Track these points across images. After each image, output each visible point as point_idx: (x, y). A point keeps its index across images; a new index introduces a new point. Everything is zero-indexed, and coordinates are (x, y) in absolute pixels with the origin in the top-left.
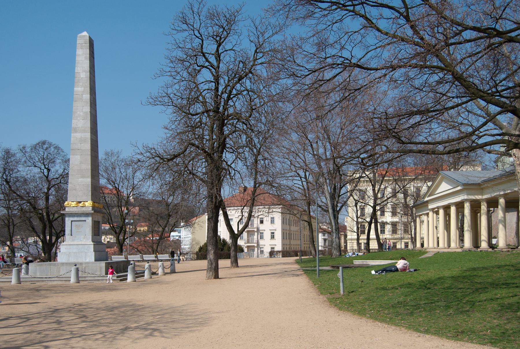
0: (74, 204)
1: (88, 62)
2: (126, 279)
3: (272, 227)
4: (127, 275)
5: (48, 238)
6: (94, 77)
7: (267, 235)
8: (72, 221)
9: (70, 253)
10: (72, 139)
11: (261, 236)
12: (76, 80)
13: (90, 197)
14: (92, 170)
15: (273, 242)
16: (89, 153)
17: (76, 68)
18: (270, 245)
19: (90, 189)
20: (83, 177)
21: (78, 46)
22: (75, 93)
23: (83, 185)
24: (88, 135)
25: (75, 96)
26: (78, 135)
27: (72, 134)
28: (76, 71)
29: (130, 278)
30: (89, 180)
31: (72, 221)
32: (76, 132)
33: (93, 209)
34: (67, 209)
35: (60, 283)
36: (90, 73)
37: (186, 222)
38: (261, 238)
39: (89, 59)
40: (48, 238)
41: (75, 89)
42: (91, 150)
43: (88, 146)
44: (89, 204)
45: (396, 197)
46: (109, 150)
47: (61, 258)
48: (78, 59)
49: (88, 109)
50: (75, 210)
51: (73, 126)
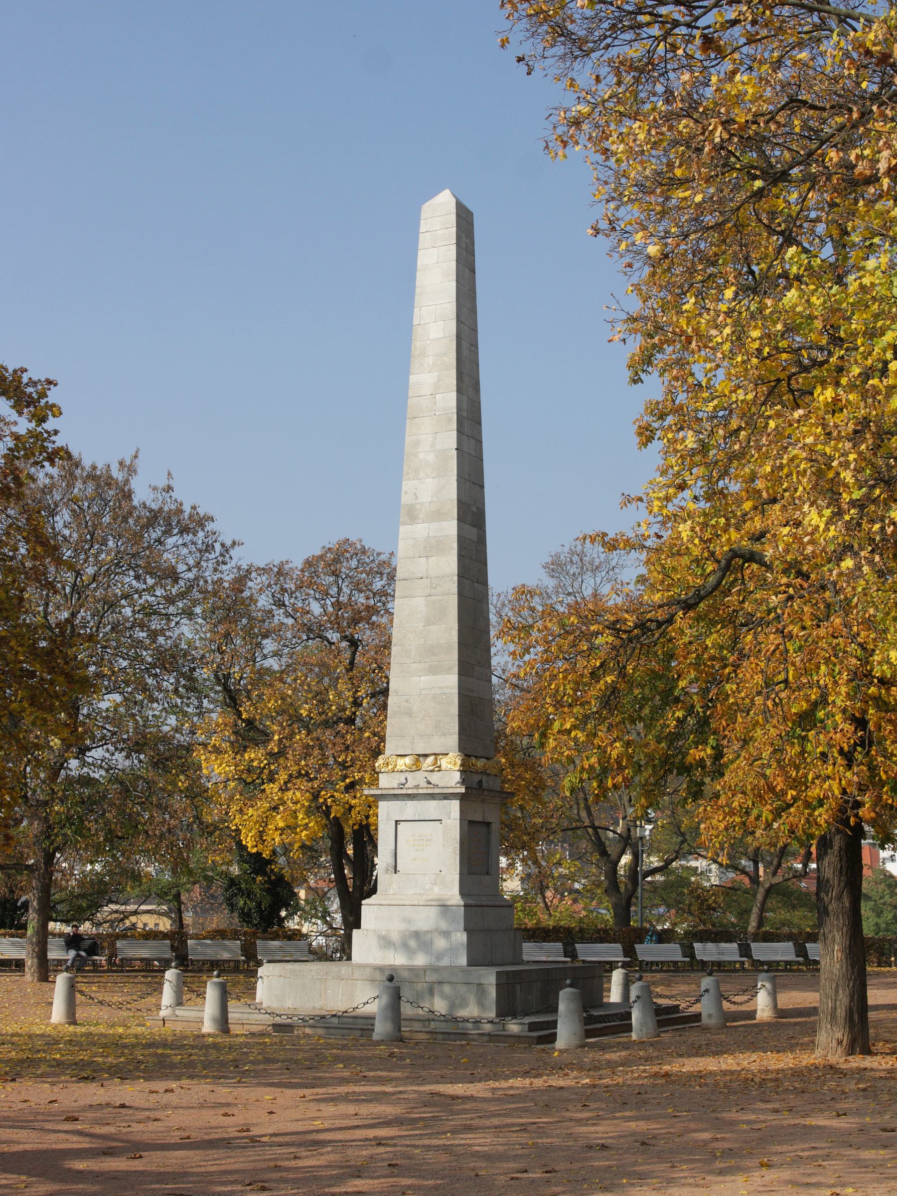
2: (552, 1038)
4: (554, 1024)
12: (417, 344)
13: (452, 740)
16: (453, 586)
19: (455, 710)
20: (434, 670)
22: (411, 394)
24: (450, 528)
25: (410, 401)
26: (421, 530)
27: (402, 529)
28: (416, 321)
29: (566, 1032)
32: (413, 518)
37: (287, 905)
41: (413, 379)
42: (460, 576)
44: (452, 764)
45: (665, 861)
46: (637, 440)
49: (450, 440)
51: (405, 499)
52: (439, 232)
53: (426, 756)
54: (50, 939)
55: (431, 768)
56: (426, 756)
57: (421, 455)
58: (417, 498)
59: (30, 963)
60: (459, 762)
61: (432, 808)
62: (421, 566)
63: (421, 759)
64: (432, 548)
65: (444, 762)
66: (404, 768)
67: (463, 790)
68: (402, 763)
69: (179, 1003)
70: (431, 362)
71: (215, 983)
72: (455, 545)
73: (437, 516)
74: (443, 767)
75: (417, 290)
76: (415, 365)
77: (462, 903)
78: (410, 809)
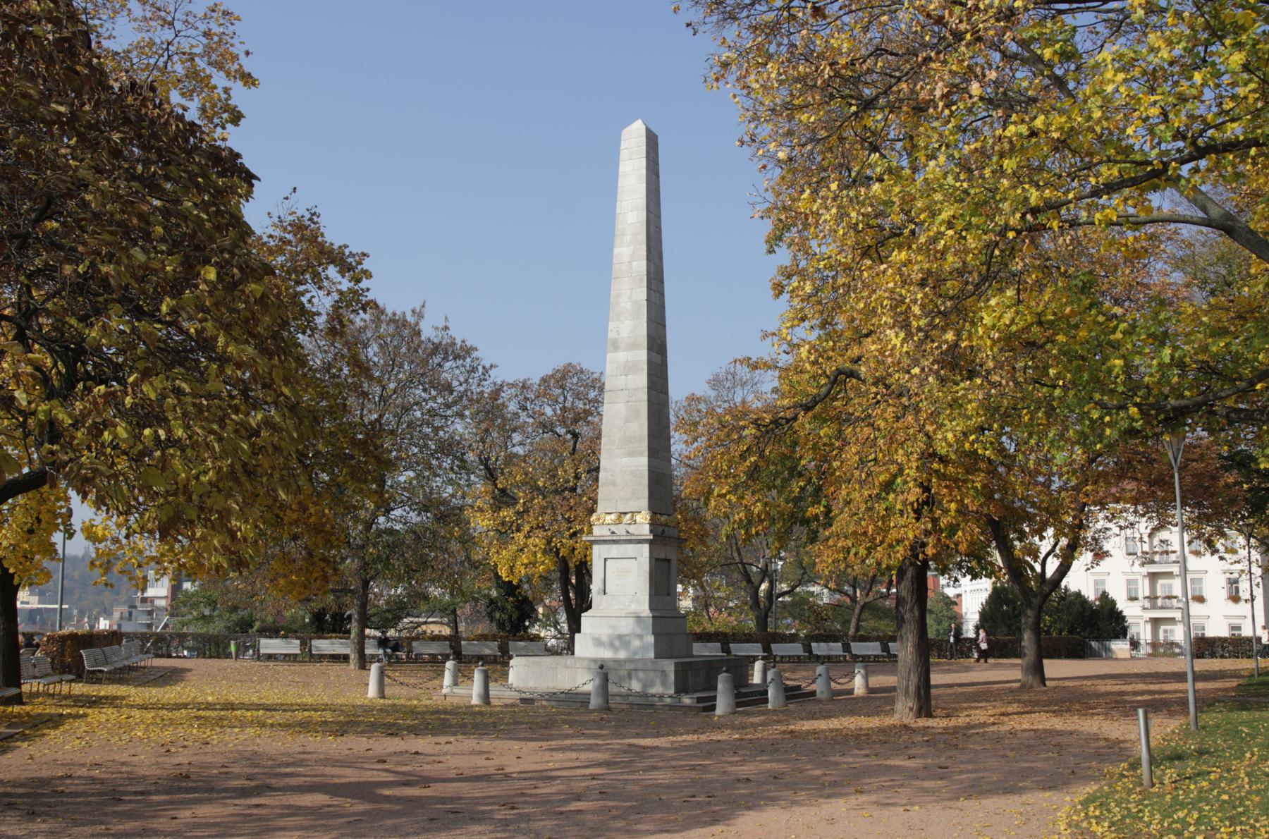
2: (713, 708)
4: (715, 697)
6: (659, 228)
12: (619, 227)
13: (644, 503)
14: (651, 388)
20: (631, 454)
27: (609, 356)
29: (723, 704)
30: (643, 461)
36: (648, 211)
39: (646, 453)
41: (616, 251)
43: (641, 380)
44: (644, 519)
49: (642, 293)
51: (611, 335)
61: (630, 549)
64: (629, 369)
65: (638, 518)
68: (609, 519)
69: (455, 684)
76: (617, 242)
78: (615, 550)
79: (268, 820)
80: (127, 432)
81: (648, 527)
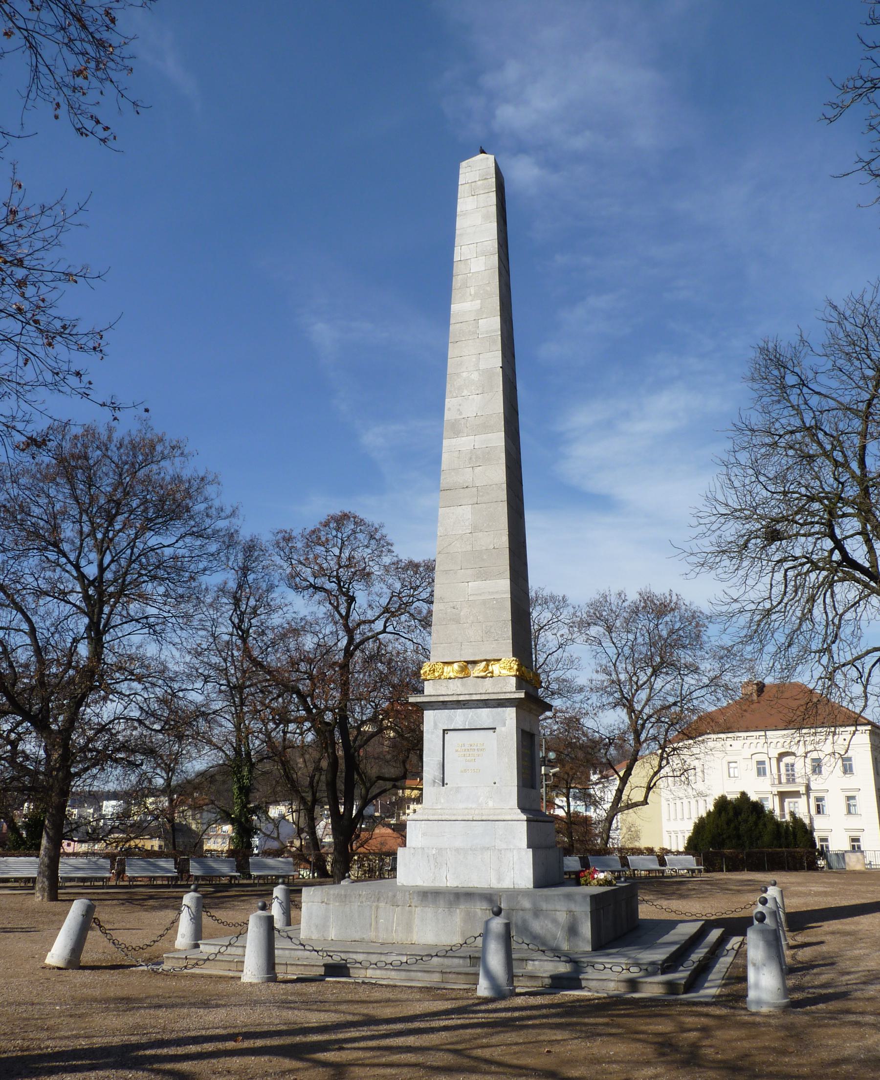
0: (451, 671)
1: (494, 226)
3: (849, 782)
5: (342, 809)
7: (835, 804)
8: (444, 730)
9: (440, 850)
10: (445, 457)
11: (818, 806)
12: (457, 281)
15: (853, 822)
17: (457, 250)
18: (847, 830)
20: (483, 575)
21: (462, 190)
23: (484, 602)
24: (498, 439)
27: (445, 442)
31: (444, 730)
32: (457, 433)
33: (519, 687)
34: (429, 688)
35: (586, 1020)
38: (819, 812)
40: (342, 809)
41: (454, 308)
47: (412, 869)
48: (462, 224)
49: (495, 359)
50: (455, 690)
52: (479, 183)
53: (475, 663)
54: (514, 962)
55: (483, 674)
56: (475, 663)
57: (465, 375)
58: (461, 414)
59: (42, 883)
60: (516, 667)
61: (485, 716)
62: (467, 476)
63: (470, 666)
64: (477, 458)
65: (496, 668)
66: (452, 675)
67: (522, 695)
68: (451, 671)
69: (198, 934)
70: (473, 292)
71: (260, 917)
72: (503, 455)
73: (484, 428)
74: (496, 673)
75: (457, 232)
76: (455, 295)
77: (524, 817)
78: (460, 717)
79: (662, 1062)
80: (705, 1055)
81: (513, 680)
